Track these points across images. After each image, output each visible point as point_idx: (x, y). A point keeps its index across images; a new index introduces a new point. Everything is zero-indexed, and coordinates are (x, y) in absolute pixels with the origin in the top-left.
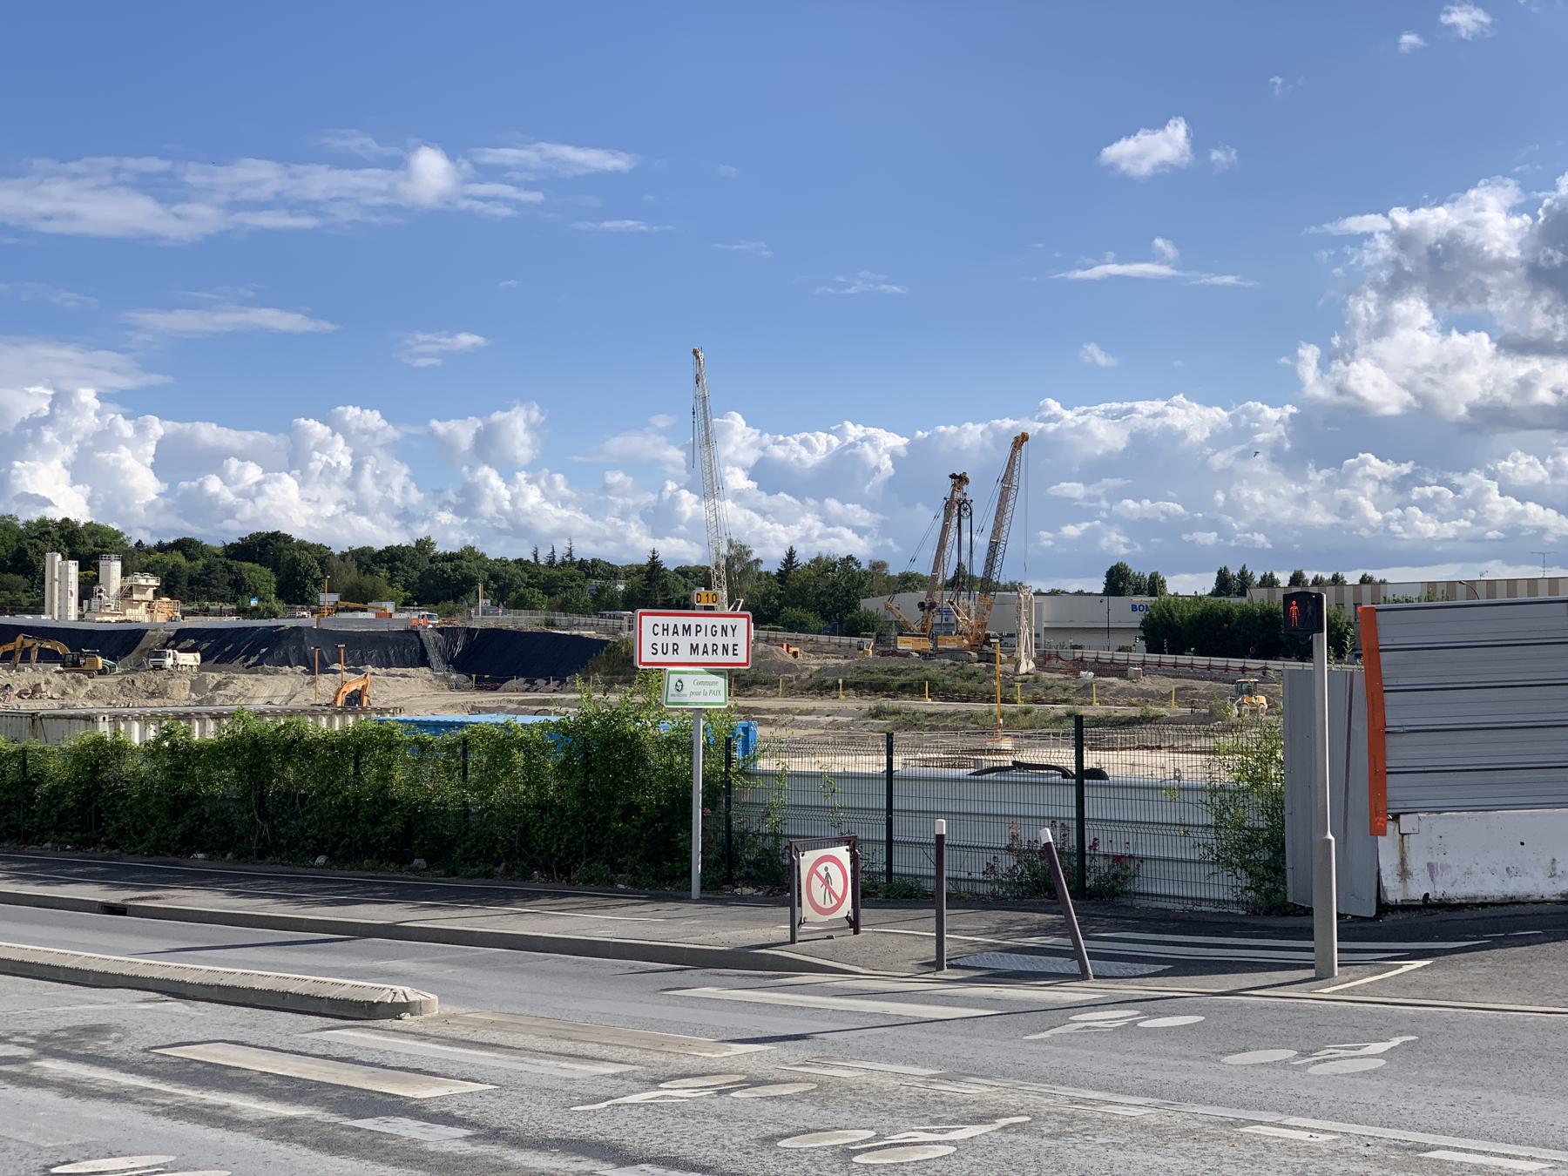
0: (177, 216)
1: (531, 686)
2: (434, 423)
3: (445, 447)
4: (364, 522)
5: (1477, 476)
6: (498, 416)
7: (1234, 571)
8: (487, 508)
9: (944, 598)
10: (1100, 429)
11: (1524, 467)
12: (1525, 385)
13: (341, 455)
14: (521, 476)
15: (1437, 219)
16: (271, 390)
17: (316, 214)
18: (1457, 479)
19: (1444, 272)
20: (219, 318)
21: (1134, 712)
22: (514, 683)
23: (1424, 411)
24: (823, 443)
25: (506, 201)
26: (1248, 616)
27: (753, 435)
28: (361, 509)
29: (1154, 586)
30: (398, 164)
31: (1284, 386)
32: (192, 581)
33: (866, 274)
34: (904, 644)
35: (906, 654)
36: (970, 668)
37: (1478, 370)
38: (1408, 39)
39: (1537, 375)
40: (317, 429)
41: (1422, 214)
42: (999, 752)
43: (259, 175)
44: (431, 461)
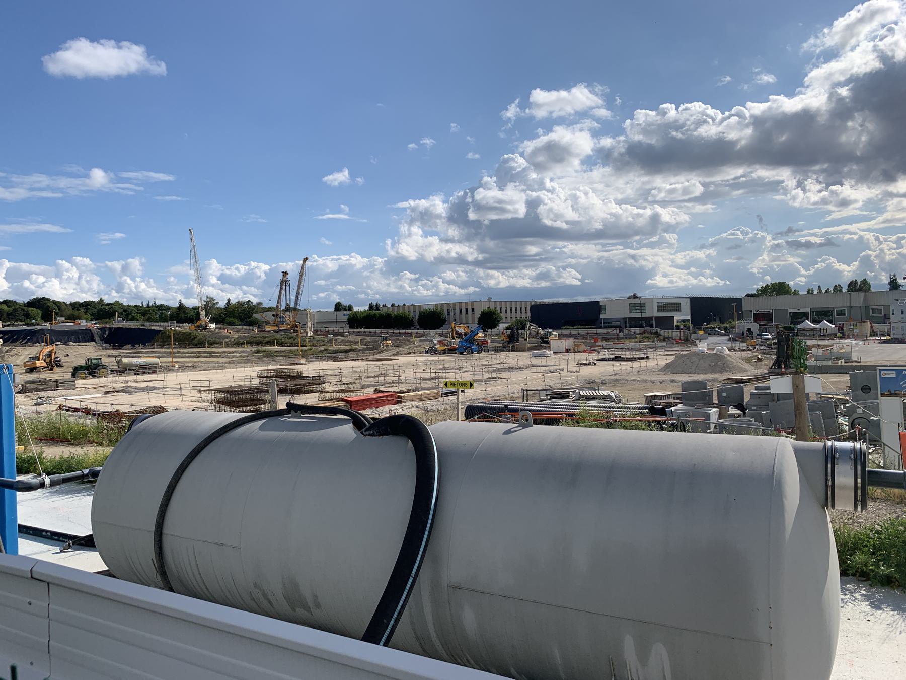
0: (11, 192)
1: (133, 347)
2: (107, 263)
3: (112, 270)
4: (84, 295)
5: (436, 278)
6: (130, 260)
7: (374, 304)
8: (126, 290)
9: (281, 314)
10: (329, 264)
11: (449, 275)
12: (448, 252)
13: (75, 273)
14: (138, 279)
15: (423, 203)
16: (47, 252)
17: (62, 193)
18: (431, 279)
19: (425, 218)
20: (29, 227)
21: (347, 348)
22: (127, 346)
23: (421, 260)
24: (243, 269)
25: (131, 190)
26: (381, 316)
27: (220, 266)
28: (82, 291)
29: (350, 308)
30: (87, 176)
31: (382, 253)
32: (8, 315)
33: (253, 215)
34: (268, 328)
35: (269, 332)
36: (290, 335)
37: (436, 248)
38: (412, 146)
39: (451, 249)
40: (66, 264)
41: (417, 202)
42: (300, 364)
43: (42, 180)
44: (106, 275)
